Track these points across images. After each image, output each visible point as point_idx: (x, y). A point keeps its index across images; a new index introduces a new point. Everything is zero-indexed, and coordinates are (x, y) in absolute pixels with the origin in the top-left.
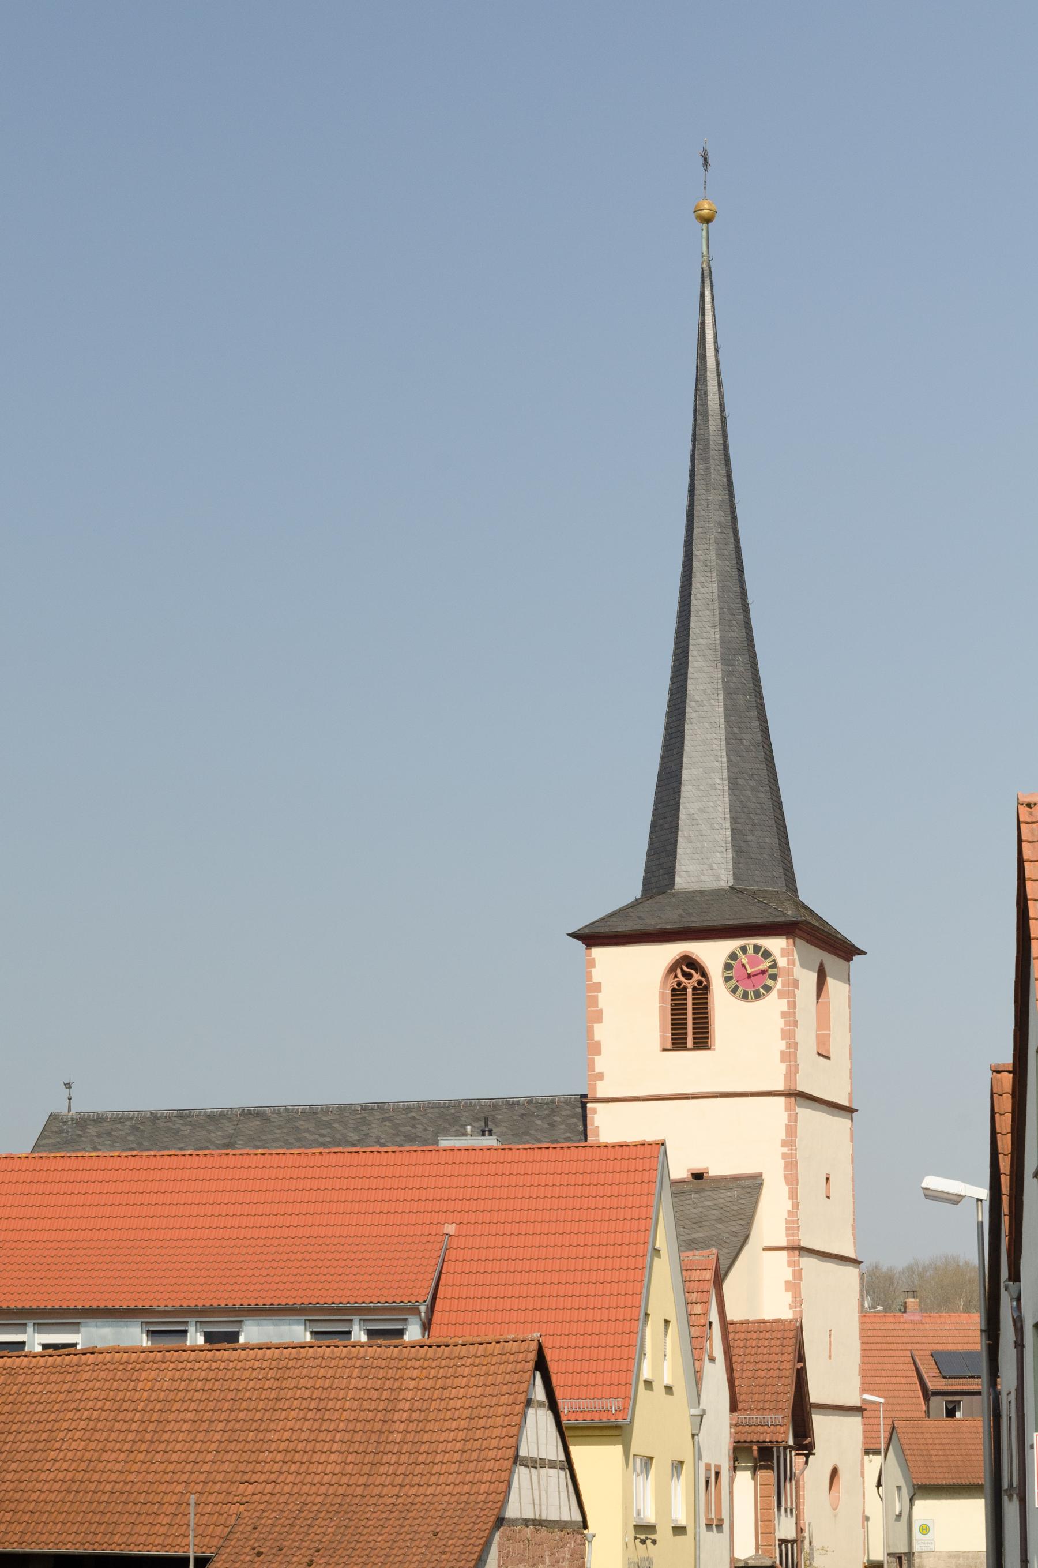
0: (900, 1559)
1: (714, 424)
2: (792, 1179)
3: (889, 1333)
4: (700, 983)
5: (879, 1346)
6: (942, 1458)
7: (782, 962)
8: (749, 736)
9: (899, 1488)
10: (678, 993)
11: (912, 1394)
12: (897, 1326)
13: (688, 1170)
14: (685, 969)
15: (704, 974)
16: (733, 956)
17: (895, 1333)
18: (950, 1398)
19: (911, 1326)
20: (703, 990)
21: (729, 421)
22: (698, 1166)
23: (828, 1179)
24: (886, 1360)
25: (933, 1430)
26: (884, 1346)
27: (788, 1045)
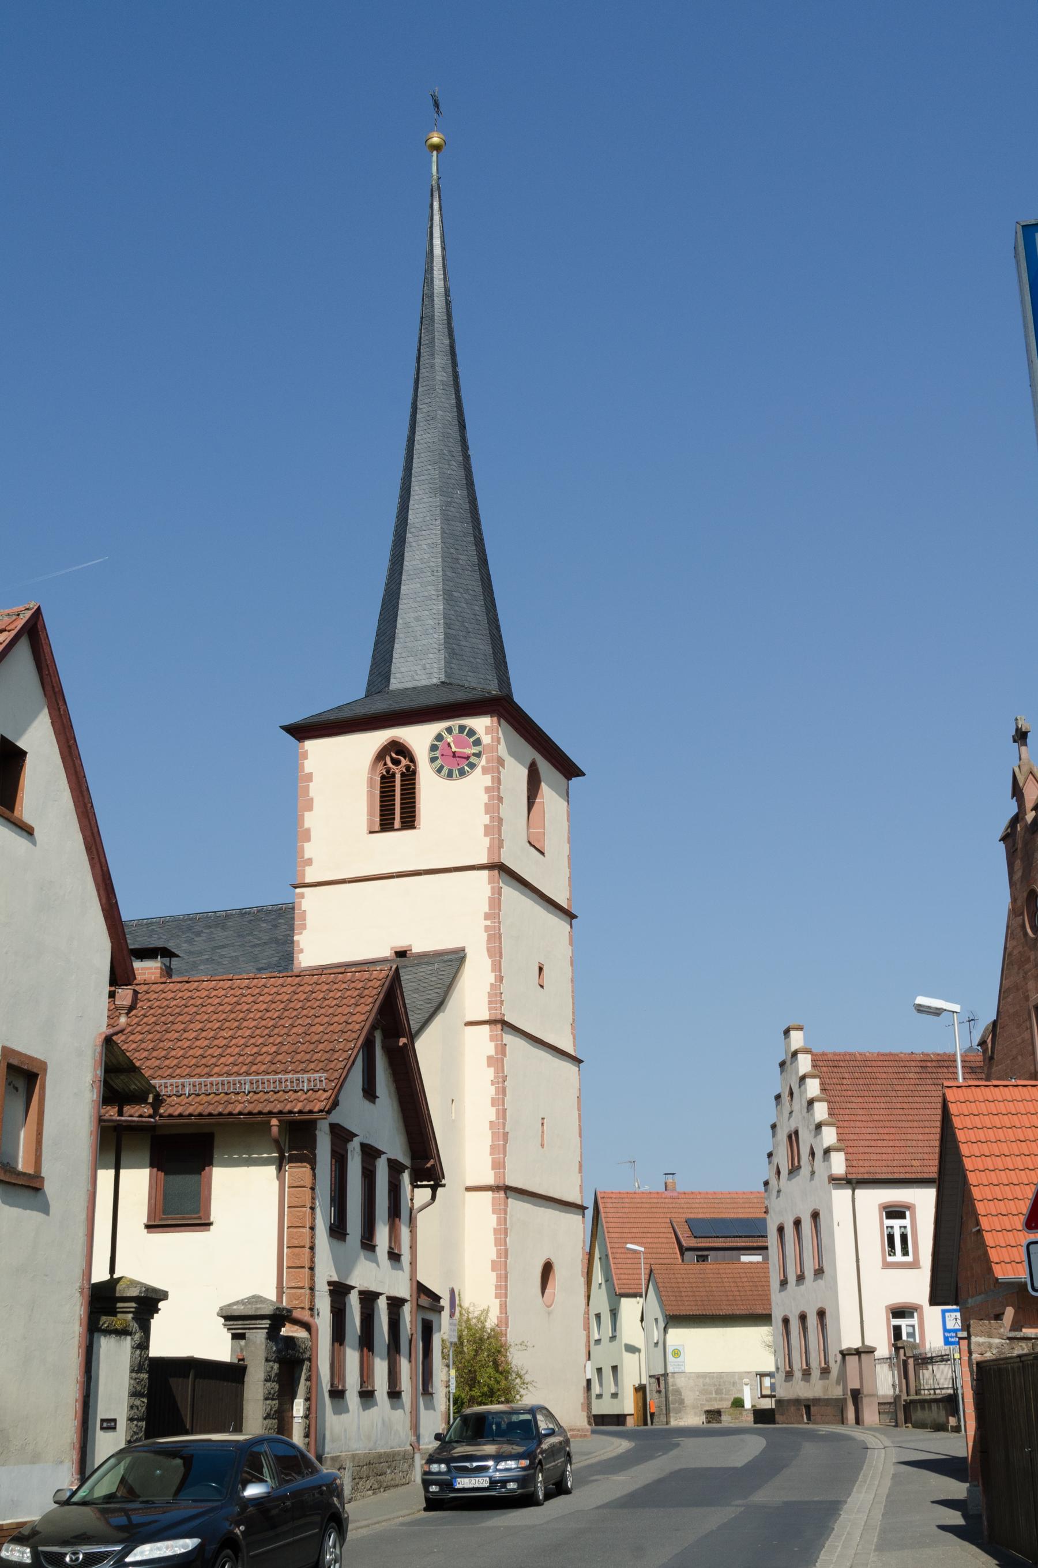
0: (658, 1379)
1: (439, 302)
2: (496, 952)
3: (655, 1205)
4: (408, 768)
5: (645, 1215)
6: (690, 1294)
7: (486, 739)
8: (466, 558)
9: (656, 1320)
10: (387, 780)
11: (671, 1251)
12: (660, 1201)
13: (392, 949)
14: (394, 755)
15: (412, 760)
16: (439, 737)
17: (659, 1205)
18: (700, 1253)
19: (670, 1201)
20: (410, 776)
21: (453, 305)
22: (401, 944)
23: (541, 969)
24: (651, 1225)
25: (682, 1272)
26: (649, 1215)
27: (492, 819)
